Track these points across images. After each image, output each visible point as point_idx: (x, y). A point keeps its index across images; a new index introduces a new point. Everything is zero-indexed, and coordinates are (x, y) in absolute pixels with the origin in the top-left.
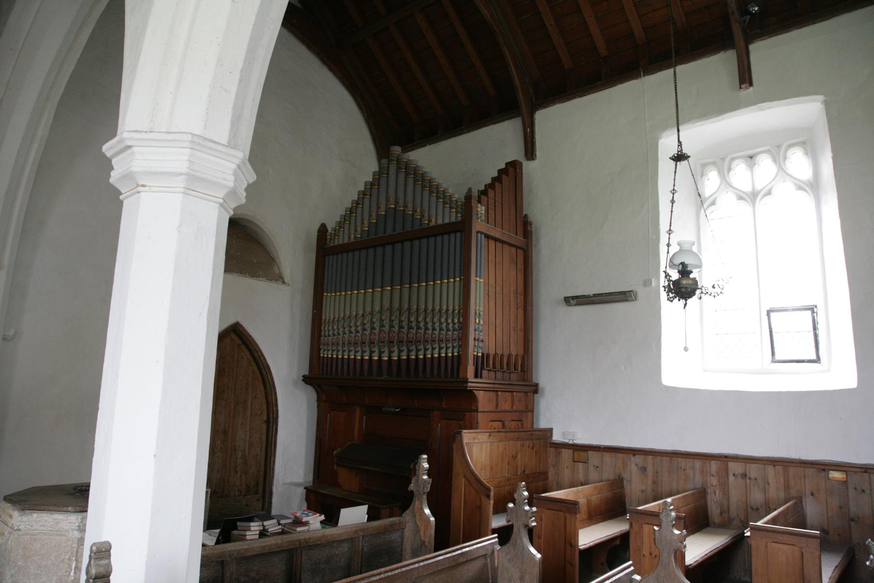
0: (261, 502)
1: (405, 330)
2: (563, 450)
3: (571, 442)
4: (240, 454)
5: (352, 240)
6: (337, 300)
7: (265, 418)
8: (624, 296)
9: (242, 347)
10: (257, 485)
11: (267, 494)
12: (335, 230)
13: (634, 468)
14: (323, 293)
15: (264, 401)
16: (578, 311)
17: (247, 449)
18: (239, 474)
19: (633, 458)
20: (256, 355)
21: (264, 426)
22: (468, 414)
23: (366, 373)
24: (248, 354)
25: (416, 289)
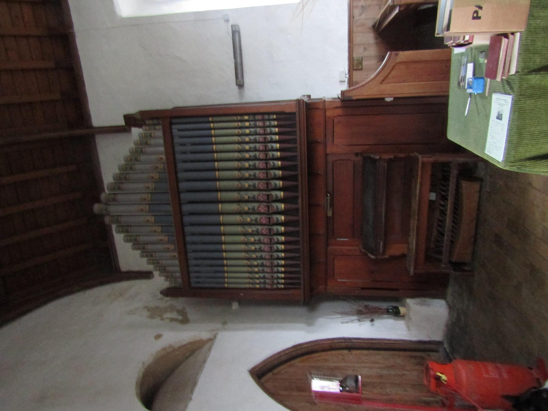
0: (431, 353)
1: (264, 254)
2: (354, 80)
3: (347, 76)
4: (385, 372)
5: (176, 254)
6: (232, 280)
7: (346, 352)
8: (235, 33)
9: (275, 371)
10: (414, 357)
11: (421, 347)
12: (167, 277)
13: (363, 16)
14: (225, 288)
15: (329, 353)
16: (247, 80)
17: (378, 365)
18: (406, 372)
19: (356, 18)
20: (284, 358)
21: (354, 352)
22: (328, 114)
23: (297, 255)
24: (281, 367)
25: (217, 138)
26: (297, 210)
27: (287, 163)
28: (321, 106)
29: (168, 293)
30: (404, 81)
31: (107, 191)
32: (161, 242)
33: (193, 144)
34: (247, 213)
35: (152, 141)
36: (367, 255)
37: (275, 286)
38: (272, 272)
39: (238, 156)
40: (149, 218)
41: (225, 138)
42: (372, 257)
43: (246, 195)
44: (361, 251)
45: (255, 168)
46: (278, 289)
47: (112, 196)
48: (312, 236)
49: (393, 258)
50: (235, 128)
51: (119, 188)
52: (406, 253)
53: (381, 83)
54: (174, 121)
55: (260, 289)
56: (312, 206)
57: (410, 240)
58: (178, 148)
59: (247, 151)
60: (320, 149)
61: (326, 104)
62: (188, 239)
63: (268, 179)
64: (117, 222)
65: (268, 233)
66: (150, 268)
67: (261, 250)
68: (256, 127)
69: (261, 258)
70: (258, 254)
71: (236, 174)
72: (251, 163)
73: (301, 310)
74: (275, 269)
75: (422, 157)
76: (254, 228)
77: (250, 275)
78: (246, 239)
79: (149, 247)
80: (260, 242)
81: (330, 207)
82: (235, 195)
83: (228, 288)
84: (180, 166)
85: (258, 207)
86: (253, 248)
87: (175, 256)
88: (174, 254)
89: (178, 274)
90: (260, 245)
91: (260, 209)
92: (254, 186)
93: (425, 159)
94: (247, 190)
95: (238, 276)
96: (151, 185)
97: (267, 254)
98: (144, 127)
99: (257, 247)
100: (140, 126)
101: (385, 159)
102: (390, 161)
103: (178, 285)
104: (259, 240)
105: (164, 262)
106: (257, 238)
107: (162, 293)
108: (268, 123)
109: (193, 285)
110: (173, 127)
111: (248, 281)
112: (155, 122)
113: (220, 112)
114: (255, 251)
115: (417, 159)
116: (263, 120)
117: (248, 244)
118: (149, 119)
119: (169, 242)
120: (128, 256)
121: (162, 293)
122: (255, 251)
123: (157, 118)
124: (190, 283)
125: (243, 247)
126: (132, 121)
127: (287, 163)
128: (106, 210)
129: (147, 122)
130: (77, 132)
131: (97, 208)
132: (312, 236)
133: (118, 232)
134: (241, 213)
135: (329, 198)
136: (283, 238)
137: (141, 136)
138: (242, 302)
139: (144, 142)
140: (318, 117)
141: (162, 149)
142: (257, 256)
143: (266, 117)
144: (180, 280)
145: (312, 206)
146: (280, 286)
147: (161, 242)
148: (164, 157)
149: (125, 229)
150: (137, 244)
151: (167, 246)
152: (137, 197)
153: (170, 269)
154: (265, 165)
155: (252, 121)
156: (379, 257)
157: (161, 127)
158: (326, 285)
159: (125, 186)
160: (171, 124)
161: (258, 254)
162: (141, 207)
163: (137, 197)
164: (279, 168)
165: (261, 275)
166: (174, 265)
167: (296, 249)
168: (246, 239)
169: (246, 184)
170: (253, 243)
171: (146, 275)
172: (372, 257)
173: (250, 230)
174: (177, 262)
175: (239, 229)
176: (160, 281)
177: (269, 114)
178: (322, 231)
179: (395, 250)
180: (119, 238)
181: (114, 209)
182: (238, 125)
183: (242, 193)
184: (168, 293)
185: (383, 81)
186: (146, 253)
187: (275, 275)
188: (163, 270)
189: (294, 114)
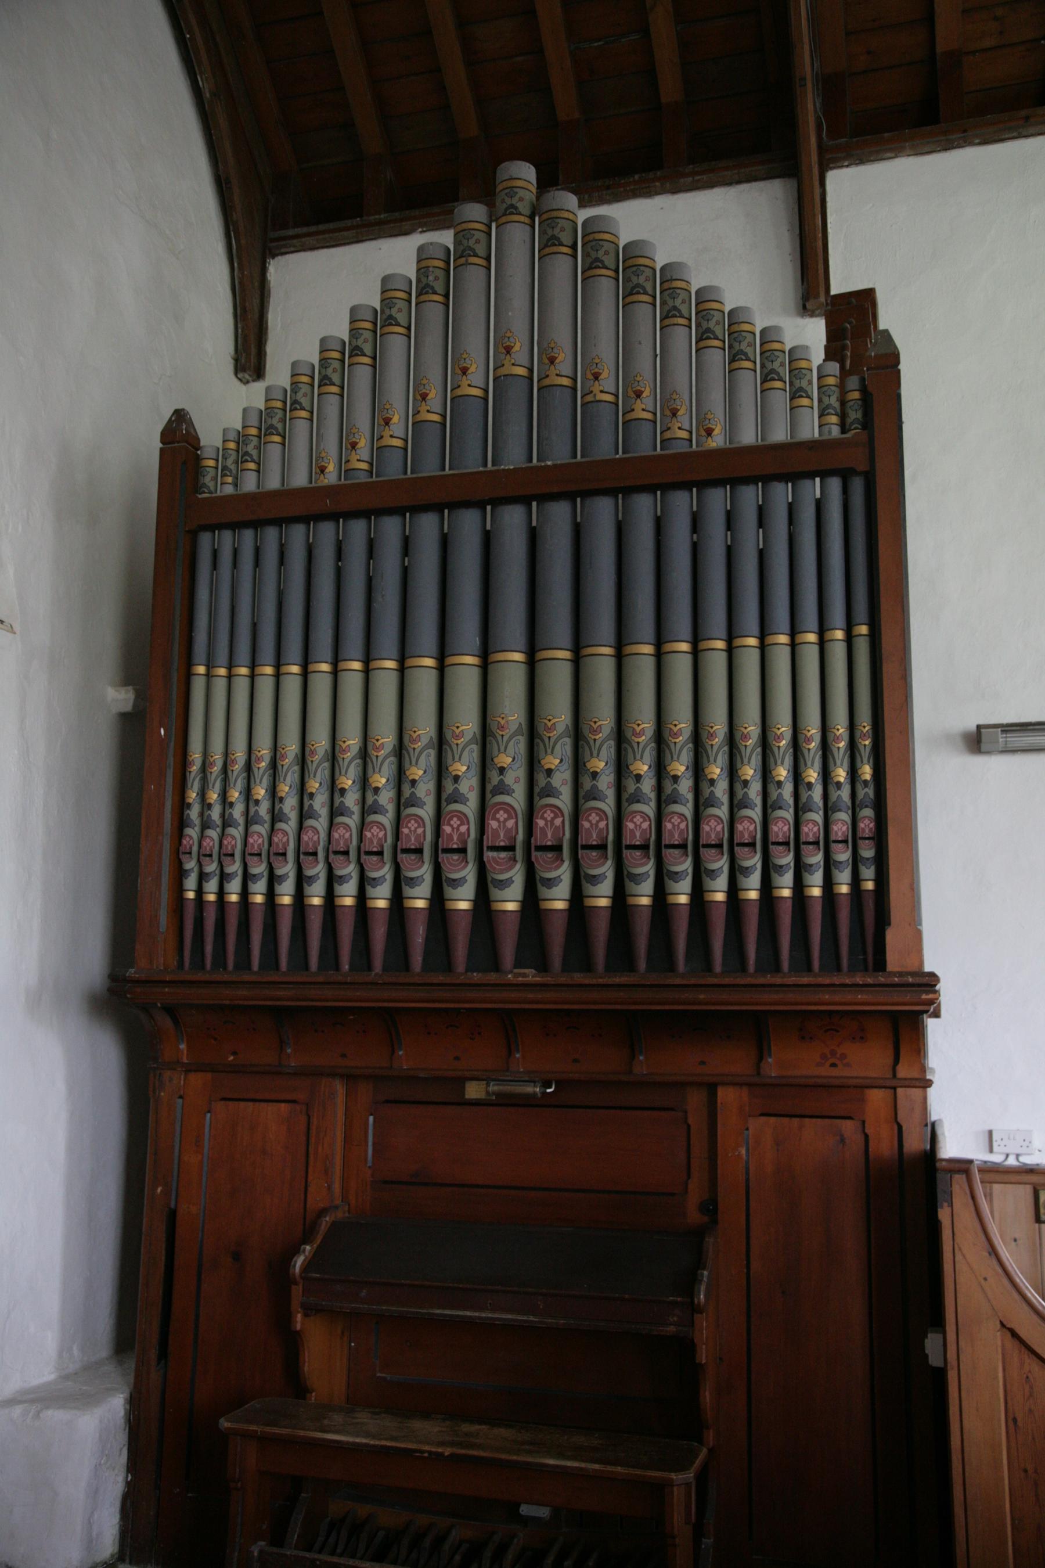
5: (331, 476)
26: (496, 966)
27: (642, 928)
28: (904, 1071)
29: (179, 438)
30: (1012, 1421)
31: (583, 215)
32: (380, 419)
33: (762, 556)
34: (485, 762)
35: (779, 400)
36: (305, 1242)
37: (190, 864)
38: (304, 854)
39: (746, 737)
40: (476, 375)
41: (780, 684)
42: (299, 1261)
43: (557, 760)
44: (322, 1212)
45: (663, 800)
46: (180, 874)
47: (566, 238)
48: (389, 1022)
49: (292, 1344)
50: (852, 727)
51: (593, 264)
52: (313, 1397)
53: (1002, 1324)
54: (857, 485)
55: (182, 804)
56: (509, 1024)
57: (363, 1417)
58: (750, 496)
59: (732, 772)
60: (729, 1060)
61: (916, 1092)
62: (391, 528)
63: (620, 850)
64: (463, 251)
65: (403, 844)
66: (278, 374)
67: (335, 812)
68: (829, 809)
69: (304, 814)
70: (320, 803)
71: (644, 724)
72: (685, 787)
73: (93, 961)
74: (259, 869)
75: (688, 1485)
76: (425, 790)
77: (238, 767)
78: (349, 755)
79: (363, 375)
80: (367, 809)
81: (498, 1095)
82: (558, 714)
83: (188, 676)
84: (682, 503)
85: (509, 809)
86: (348, 781)
87: (323, 470)
88: (331, 468)
89: (250, 484)
90: (356, 809)
91: (502, 815)
92: (594, 795)
93: (677, 1494)
94: (578, 766)
95: (237, 713)
96: (561, 374)
97: (323, 835)
98: (834, 367)
99: (351, 800)
100: (832, 352)
101: (692, 1324)
102: (686, 1346)
103: (207, 480)
104: (376, 809)
105: (301, 428)
106: (386, 798)
107: (180, 416)
108: (843, 855)
109: (205, 540)
110: (835, 484)
111: (218, 758)
112: (855, 415)
113: (888, 669)
114: (334, 789)
115: (682, 1468)
116: (855, 839)
117: (362, 765)
118: (864, 390)
119: (379, 451)
120: (326, 289)
121: (180, 416)
122: (334, 789)
123: (867, 423)
124: (211, 528)
125: (352, 742)
126: (853, 320)
127: (642, 928)
128: (512, 209)
129: (853, 382)
130: (810, 106)
131: (525, 173)
132: (389, 1022)
133: (422, 255)
134: (486, 735)
135: (530, 1089)
136: (419, 901)
137: (796, 355)
138: (132, 726)
139: (775, 364)
140: (866, 1060)
141: (748, 436)
142: (311, 796)
143: (868, 852)
144: (229, 490)
145: (509, 1024)
146: (191, 883)
147: (380, 419)
148: (718, 441)
149: (436, 281)
150: (373, 327)
151: (363, 443)
152: (605, 349)
153: (274, 452)
154: (713, 839)
155: (853, 795)
156: (297, 1291)
157: (835, 432)
158: (188, 1070)
159: (605, 287)
160: (845, 475)
161: (320, 803)
162: (520, 349)
163: (605, 349)
164: (660, 893)
165: (238, 812)
166: (289, 468)
167: (249, 951)
168: (349, 755)
169: (601, 763)
170: (364, 782)
171: (250, 357)
172: (299, 1261)
173: (420, 771)
174: (300, 479)
175: (424, 728)
176: (224, 407)
177: (881, 862)
178: (405, 1059)
179: (325, 1355)
180: (397, 255)
181: (518, 237)
182: (838, 739)
183: (608, 751)
184: (179, 438)
185: (1014, 1334)
186: (336, 362)
187: (235, 867)
188: (268, 425)
189: (880, 964)
